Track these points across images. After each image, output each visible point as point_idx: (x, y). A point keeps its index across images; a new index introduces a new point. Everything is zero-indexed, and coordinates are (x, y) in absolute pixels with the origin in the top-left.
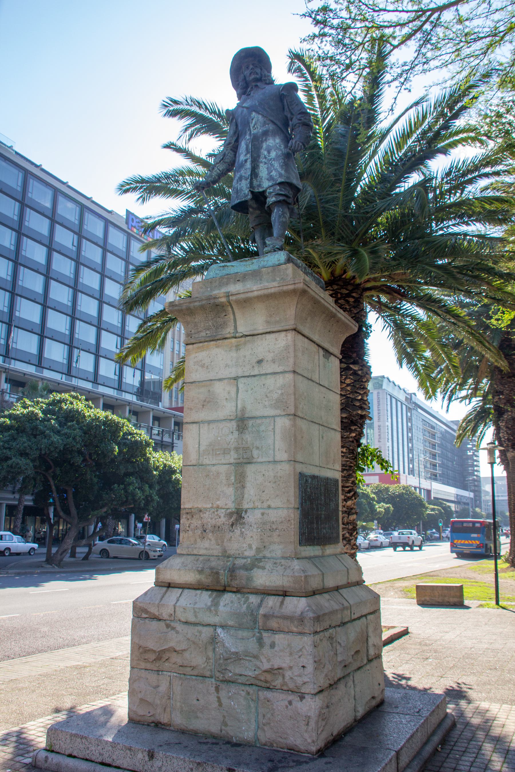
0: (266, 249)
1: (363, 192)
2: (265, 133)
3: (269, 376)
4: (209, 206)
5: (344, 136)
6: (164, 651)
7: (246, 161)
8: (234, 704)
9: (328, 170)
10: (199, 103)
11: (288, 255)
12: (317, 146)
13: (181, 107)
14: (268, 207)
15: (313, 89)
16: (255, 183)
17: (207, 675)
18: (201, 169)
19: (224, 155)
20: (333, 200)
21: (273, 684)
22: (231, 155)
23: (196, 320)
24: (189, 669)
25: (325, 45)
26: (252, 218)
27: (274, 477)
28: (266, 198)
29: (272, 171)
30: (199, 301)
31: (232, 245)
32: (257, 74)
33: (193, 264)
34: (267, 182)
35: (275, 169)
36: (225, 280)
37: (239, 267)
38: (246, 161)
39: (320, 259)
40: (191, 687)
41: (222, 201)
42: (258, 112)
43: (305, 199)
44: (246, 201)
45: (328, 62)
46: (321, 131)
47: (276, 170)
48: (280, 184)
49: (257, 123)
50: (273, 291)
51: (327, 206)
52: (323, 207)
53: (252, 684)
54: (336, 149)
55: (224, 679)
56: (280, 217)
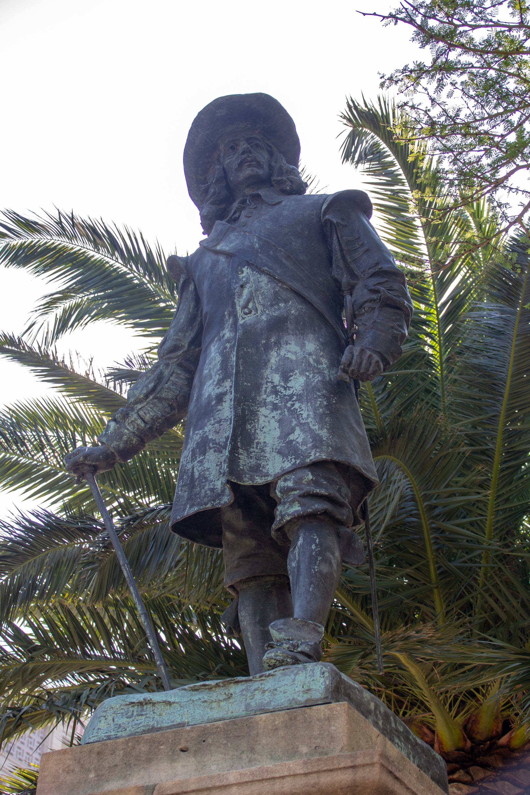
0: (270, 655)
2: (278, 326)
4: (109, 516)
5: (500, 333)
7: (220, 398)
9: (454, 427)
10: (93, 230)
11: (335, 676)
12: (423, 358)
13: (43, 239)
14: (280, 529)
15: (412, 205)
16: (245, 461)
18: (88, 411)
19: (159, 379)
20: (467, 510)
22: (176, 378)
25: (450, 95)
26: (232, 558)
28: (273, 504)
29: (293, 431)
31: (170, 631)
32: (259, 165)
33: (49, 684)
34: (278, 458)
35: (300, 425)
36: (144, 748)
37: (187, 705)
38: (220, 398)
39: (431, 682)
41: (145, 501)
42: (257, 268)
43: (384, 509)
44: (216, 512)
45: (457, 139)
46: (433, 318)
47: (304, 426)
48: (316, 465)
49: (255, 296)
51: (448, 525)
52: (437, 529)
54: (477, 368)
56: (312, 560)
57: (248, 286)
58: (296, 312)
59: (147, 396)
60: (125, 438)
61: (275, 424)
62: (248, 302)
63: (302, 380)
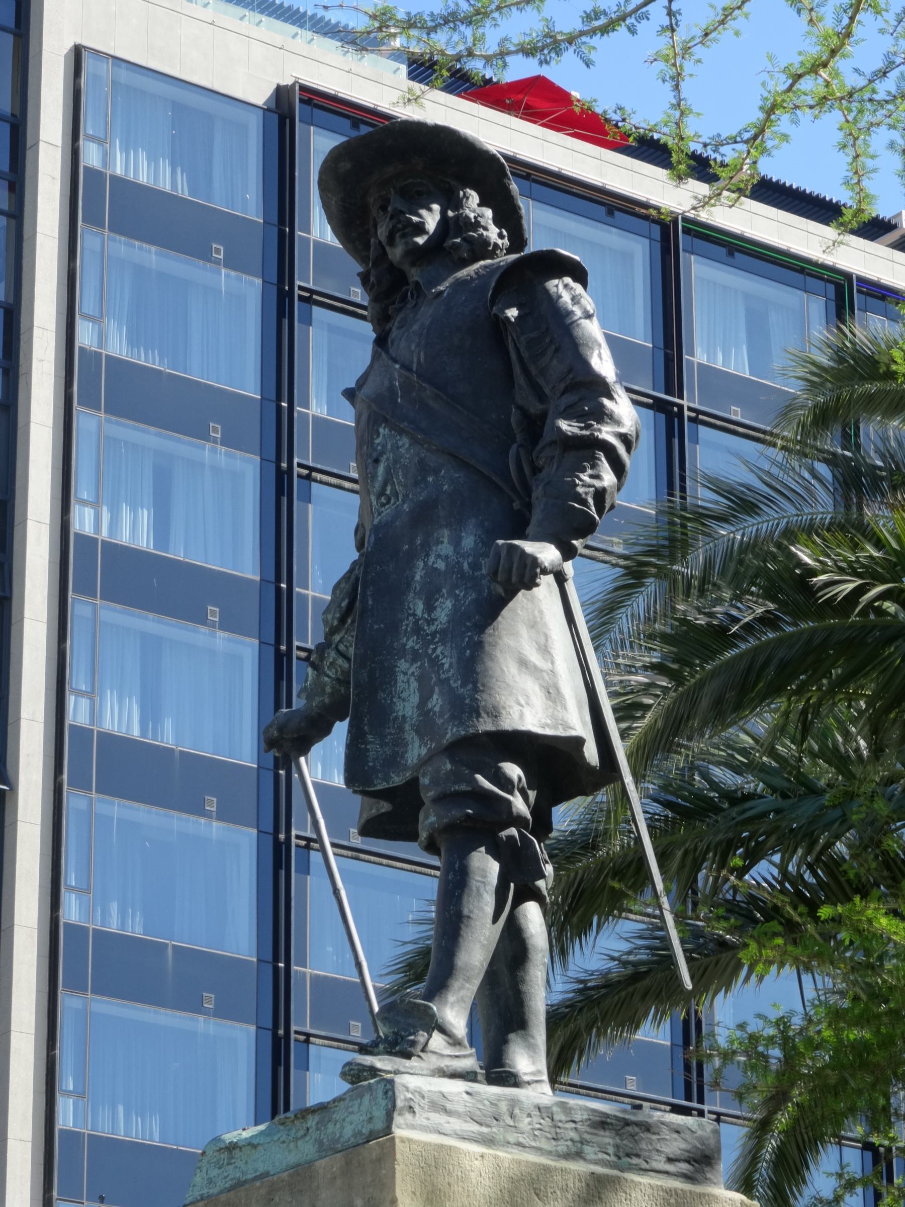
57: (384, 459)
58: (449, 486)
59: (342, 620)
60: (328, 689)
62: (385, 484)
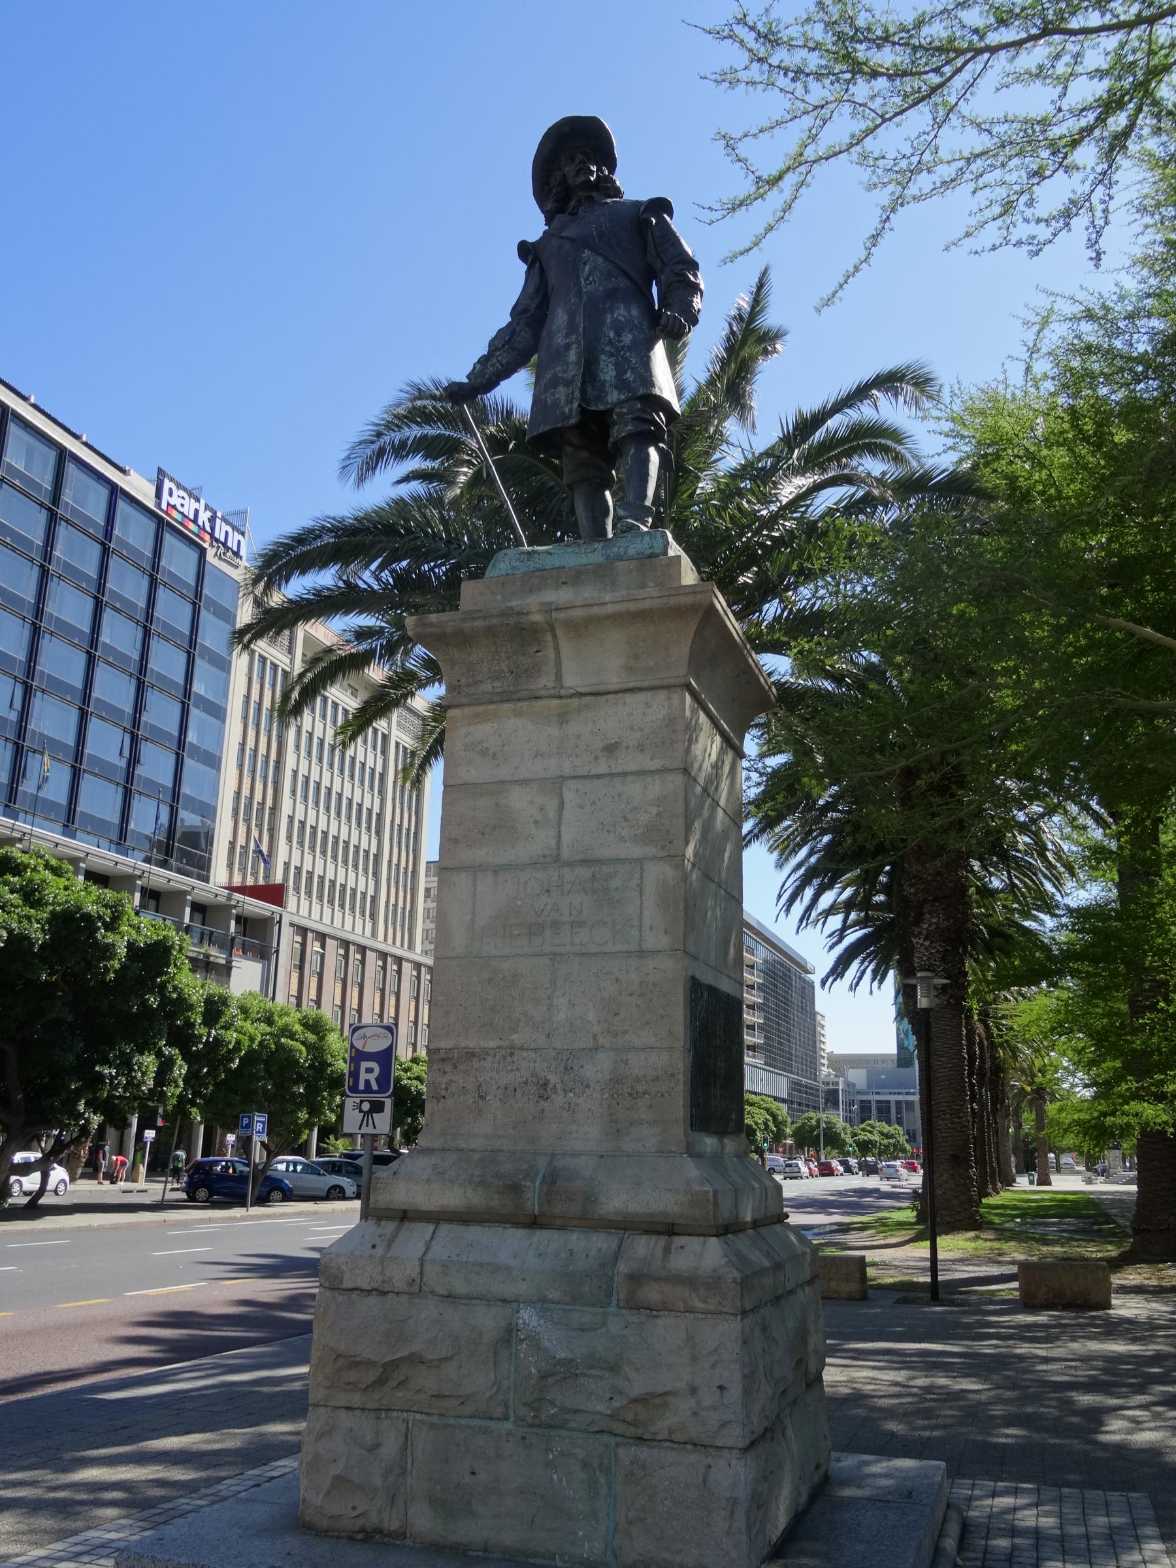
1: (434, 459)
3: (630, 779)
6: (395, 1364)
7: (567, 347)
8: (560, 1480)
14: (614, 443)
17: (495, 1415)
19: (513, 333)
21: (653, 1429)
23: (472, 658)
24: (455, 1403)
27: (641, 983)
30: (485, 618)
34: (615, 393)
35: (630, 367)
40: (458, 1445)
50: (647, 604)
53: (603, 1431)
55: (537, 1421)
59: (503, 346)
61: (611, 367)
63: (630, 336)
